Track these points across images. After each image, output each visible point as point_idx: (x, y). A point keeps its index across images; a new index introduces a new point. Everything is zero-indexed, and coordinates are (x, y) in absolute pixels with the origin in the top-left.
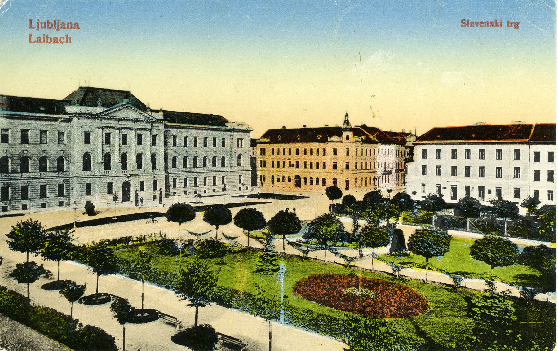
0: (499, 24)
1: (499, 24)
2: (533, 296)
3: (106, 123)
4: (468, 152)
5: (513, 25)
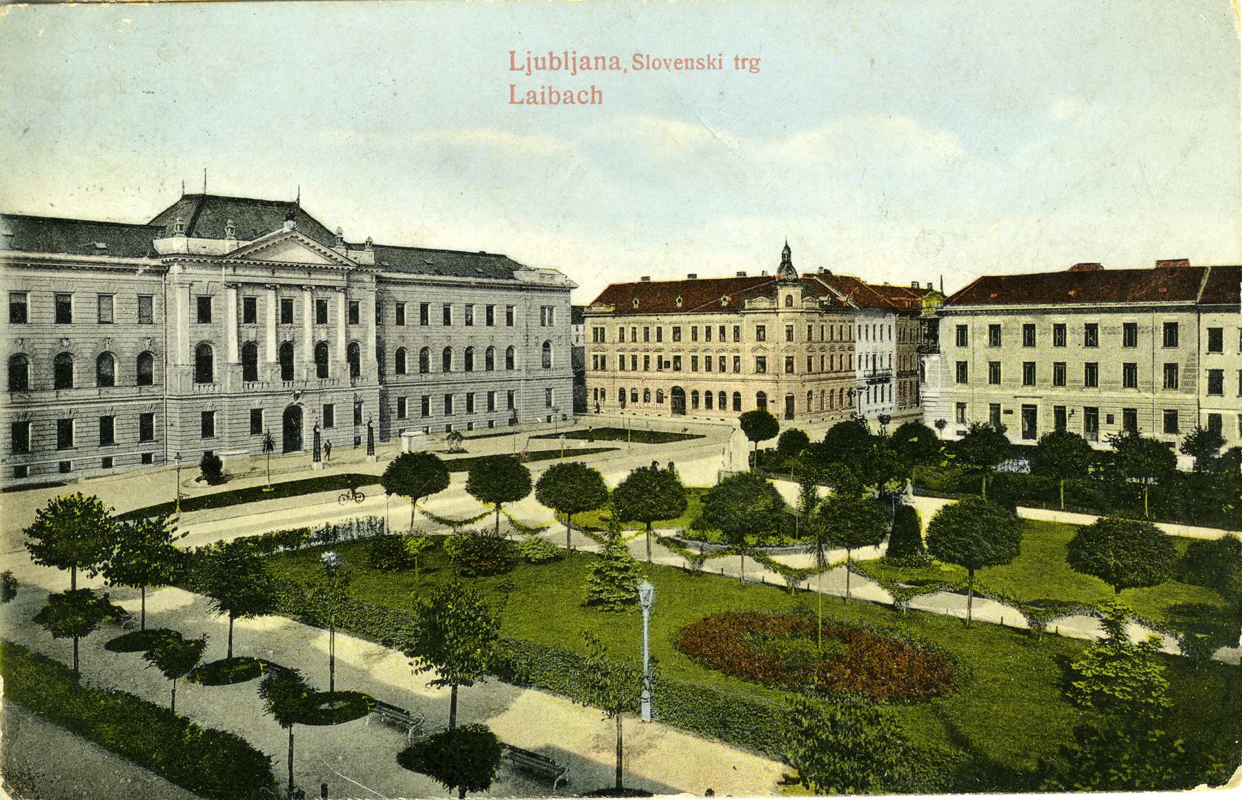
0: (717, 64)
1: (717, 64)
2: (1210, 654)
3: (244, 275)
4: (1060, 329)
5: (747, 64)
